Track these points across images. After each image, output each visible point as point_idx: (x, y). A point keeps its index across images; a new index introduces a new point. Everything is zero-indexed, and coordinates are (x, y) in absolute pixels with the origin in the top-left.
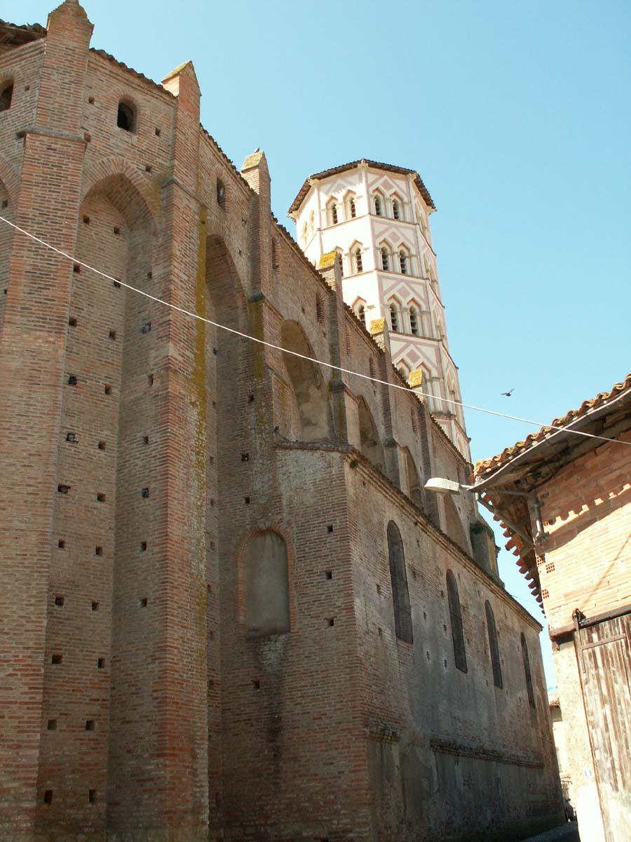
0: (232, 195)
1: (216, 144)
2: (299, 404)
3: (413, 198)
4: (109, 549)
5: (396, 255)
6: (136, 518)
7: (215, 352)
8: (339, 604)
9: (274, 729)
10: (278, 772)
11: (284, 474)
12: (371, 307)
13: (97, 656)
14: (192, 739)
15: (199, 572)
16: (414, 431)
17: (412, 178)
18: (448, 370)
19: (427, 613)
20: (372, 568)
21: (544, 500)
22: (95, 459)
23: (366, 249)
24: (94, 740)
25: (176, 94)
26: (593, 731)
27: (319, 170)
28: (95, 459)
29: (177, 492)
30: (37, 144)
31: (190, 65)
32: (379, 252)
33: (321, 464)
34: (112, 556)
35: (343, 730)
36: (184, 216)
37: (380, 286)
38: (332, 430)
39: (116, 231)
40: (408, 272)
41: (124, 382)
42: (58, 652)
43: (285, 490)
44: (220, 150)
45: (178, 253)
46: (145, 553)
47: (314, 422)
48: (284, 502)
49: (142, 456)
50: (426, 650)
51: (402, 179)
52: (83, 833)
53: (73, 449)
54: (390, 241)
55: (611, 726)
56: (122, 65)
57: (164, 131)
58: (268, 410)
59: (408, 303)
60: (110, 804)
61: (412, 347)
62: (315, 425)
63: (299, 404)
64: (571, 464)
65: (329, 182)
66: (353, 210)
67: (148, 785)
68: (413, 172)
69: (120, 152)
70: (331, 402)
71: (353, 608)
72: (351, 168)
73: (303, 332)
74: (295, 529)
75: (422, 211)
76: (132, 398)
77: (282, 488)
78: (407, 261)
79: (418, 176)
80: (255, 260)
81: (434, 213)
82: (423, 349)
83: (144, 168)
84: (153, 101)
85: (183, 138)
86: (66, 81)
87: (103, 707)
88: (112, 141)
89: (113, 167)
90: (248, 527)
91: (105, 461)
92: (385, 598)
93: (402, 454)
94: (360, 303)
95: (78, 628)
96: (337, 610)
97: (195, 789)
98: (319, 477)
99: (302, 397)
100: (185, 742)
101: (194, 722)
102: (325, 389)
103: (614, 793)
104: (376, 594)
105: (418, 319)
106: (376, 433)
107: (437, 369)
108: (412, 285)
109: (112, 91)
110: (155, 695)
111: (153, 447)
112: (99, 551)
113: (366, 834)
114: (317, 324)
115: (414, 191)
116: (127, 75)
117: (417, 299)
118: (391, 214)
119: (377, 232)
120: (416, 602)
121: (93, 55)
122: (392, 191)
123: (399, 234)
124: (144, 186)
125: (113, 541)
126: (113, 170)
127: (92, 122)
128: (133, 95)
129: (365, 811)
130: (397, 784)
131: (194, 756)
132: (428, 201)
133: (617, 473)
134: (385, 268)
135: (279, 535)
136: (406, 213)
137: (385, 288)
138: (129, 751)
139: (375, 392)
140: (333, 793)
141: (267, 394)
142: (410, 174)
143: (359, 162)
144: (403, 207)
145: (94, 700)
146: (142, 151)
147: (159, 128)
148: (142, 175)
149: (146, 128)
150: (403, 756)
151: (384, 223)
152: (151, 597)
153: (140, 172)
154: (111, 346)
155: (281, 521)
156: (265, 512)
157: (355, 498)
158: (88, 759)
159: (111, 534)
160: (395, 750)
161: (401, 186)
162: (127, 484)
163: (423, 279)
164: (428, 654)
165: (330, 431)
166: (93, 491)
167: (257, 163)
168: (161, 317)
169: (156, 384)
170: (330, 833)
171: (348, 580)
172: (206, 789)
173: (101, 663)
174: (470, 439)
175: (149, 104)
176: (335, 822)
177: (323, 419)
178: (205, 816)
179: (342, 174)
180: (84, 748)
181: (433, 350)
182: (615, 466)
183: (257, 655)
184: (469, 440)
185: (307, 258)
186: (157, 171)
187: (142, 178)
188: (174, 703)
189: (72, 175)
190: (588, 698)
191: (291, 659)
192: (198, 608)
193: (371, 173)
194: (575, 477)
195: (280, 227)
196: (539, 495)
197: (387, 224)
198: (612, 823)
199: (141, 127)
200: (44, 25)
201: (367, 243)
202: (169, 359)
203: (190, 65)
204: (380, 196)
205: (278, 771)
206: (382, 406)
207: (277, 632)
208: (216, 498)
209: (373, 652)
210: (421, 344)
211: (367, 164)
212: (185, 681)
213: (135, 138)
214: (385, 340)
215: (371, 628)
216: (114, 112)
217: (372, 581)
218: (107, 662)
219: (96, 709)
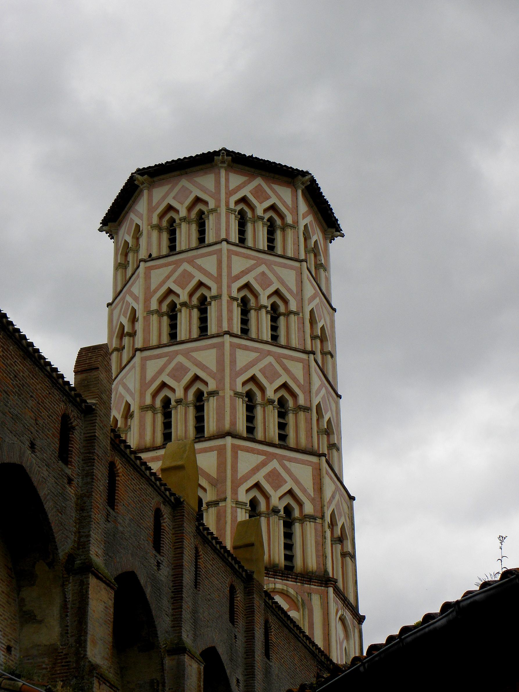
5: (263, 311)
16: (232, 620)
18: (334, 502)
32: (235, 304)
38: (64, 633)
40: (282, 340)
47: (39, 618)
54: (256, 286)
59: (276, 391)
61: (274, 464)
75: (317, 236)
81: (338, 240)
82: (293, 467)
93: (195, 666)
107: (312, 501)
108: (285, 361)
117: (292, 384)
122: (267, 204)
139: (159, 564)
151: (248, 257)
163: (305, 352)
165: (62, 635)
181: (310, 469)
197: (253, 258)
204: (246, 209)
210: (290, 460)
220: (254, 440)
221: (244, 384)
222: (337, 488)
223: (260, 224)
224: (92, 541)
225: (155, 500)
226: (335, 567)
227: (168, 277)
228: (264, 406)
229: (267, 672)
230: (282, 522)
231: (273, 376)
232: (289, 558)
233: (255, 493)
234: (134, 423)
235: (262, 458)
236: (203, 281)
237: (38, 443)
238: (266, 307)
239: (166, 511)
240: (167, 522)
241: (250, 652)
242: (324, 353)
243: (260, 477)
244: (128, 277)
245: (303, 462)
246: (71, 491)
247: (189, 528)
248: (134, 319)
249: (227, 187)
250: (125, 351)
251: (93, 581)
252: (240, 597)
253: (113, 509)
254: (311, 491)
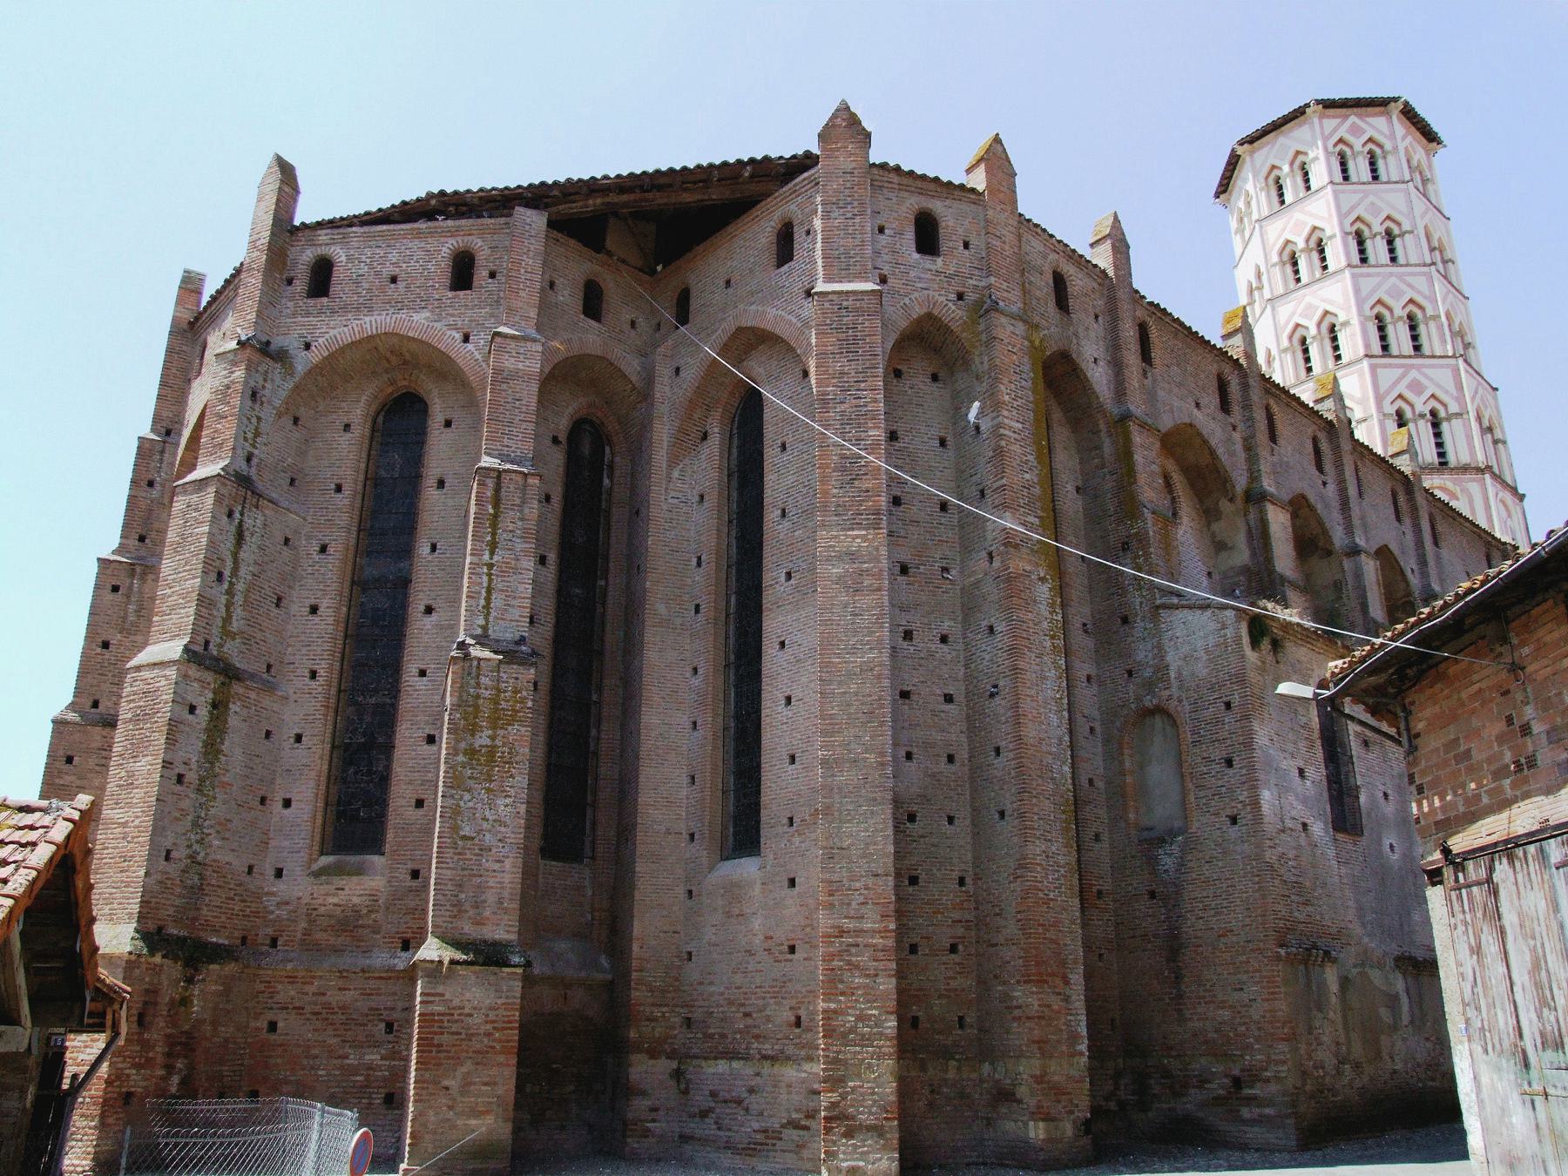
0: (1076, 288)
1: (1044, 230)
2: (1209, 524)
3: (1399, 140)
4: (963, 754)
5: (1378, 237)
6: (988, 719)
7: (1078, 489)
8: (1241, 798)
9: (1174, 946)
10: (1181, 998)
11: (1171, 640)
12: (1346, 324)
13: (956, 875)
14: (1063, 963)
15: (1063, 775)
16: (1398, 519)
17: (1395, 109)
19: (1389, 792)
20: (1290, 747)
21: (1413, 708)
22: (937, 655)
23: (1331, 238)
24: (958, 964)
25: (981, 187)
26: (1463, 984)
27: (1249, 129)
28: (937, 655)
29: (1029, 688)
30: (827, 305)
31: (997, 140)
32: (1350, 237)
33: (1213, 626)
34: (966, 762)
35: (1252, 950)
36: (1010, 348)
37: (1357, 291)
38: (1253, 555)
39: (935, 378)
41: (962, 561)
42: (914, 873)
43: (1173, 659)
44: (1052, 236)
45: (1007, 398)
46: (1000, 759)
48: (1173, 675)
49: (988, 648)
50: (1386, 842)
51: (1381, 114)
52: (954, 1059)
53: (912, 648)
55: (1479, 980)
56: (911, 173)
57: (973, 241)
58: (1146, 560)
60: (980, 1030)
62: (1231, 548)
63: (1209, 524)
64: (1433, 671)
65: (1268, 143)
66: (1307, 181)
67: (1016, 1013)
68: (1395, 100)
69: (924, 286)
70: (1252, 516)
71: (1259, 803)
72: (1297, 117)
73: (1200, 434)
74: (1188, 707)
75: (1419, 154)
76: (972, 579)
77: (1169, 658)
78: (1398, 242)
79: (1406, 104)
80: (1117, 365)
81: (1441, 151)
83: (953, 297)
84: (956, 204)
85: (998, 244)
86: (849, 215)
87: (968, 928)
88: (912, 274)
89: (917, 309)
90: (1133, 706)
91: (949, 657)
92: (1313, 782)
93: (1372, 563)
94: (1329, 319)
95: (933, 845)
96: (1240, 806)
97: (1069, 1017)
98: (1212, 641)
99: (1209, 514)
100: (1055, 967)
101: (1066, 945)
102: (1239, 501)
103: (1484, 1056)
104: (1298, 779)
105: (1422, 329)
106: (1329, 539)
108: (1408, 278)
109: (904, 209)
110: (1019, 916)
111: (999, 638)
112: (951, 759)
113: (1284, 1075)
114: (1221, 416)
115: (1400, 127)
116: (919, 183)
118: (1366, 175)
119: (1344, 210)
120: (1368, 780)
121: (875, 171)
123: (1379, 203)
124: (957, 321)
125: (966, 746)
126: (918, 311)
127: (886, 258)
128: (930, 206)
129: (1283, 1046)
130: (1335, 1014)
131: (1067, 982)
132: (1429, 136)
133: (1476, 687)
134: (1364, 260)
135: (1169, 715)
136: (1391, 168)
137: (1364, 293)
138: (996, 977)
139: (1324, 484)
140: (1245, 1023)
141: (1142, 539)
142: (1393, 104)
143: (1308, 105)
144: (1385, 158)
145: (957, 921)
146: (950, 277)
147: (967, 239)
148: (953, 308)
149: (951, 244)
150: (1345, 982)
152: (1009, 809)
153: (950, 304)
154: (943, 520)
155: (1170, 697)
156: (1150, 686)
157: (1259, 663)
158: (953, 984)
159: (963, 738)
160: (1331, 976)
161: (1378, 126)
162: (975, 681)
164: (1391, 846)
166: (938, 692)
167: (1107, 232)
168: (995, 482)
169: (997, 563)
170: (1242, 1071)
171: (1251, 768)
172: (1084, 1018)
173: (962, 882)
174: (1524, 495)
175: (950, 210)
176: (1248, 1057)
177: (1241, 539)
178: (1083, 1047)
179: (1283, 128)
180: (950, 974)
182: (1475, 677)
183: (1152, 861)
184: (1522, 497)
185: (1196, 333)
186: (971, 297)
187: (953, 312)
188: (1039, 925)
189: (869, 335)
190: (1456, 946)
191: (1190, 865)
192: (1064, 816)
193: (1329, 117)
194: (1439, 686)
195: (1151, 304)
196: (1407, 701)
197: (1359, 191)
198: (1484, 1089)
199: (944, 246)
200: (816, 150)
201: (1332, 228)
202: (1008, 533)
203: (997, 140)
204: (1347, 150)
205: (1180, 996)
206: (1338, 498)
207: (1173, 833)
208: (1093, 672)
209: (1291, 854)
211: (1321, 106)
212: (1052, 900)
213: (939, 260)
214: (1335, 405)
215: (1289, 824)
216: (910, 235)
217: (1290, 765)
218: (968, 880)
219: (960, 931)
220: (1391, 356)
221: (1352, 224)
222: (1479, 383)
223: (1400, 324)
224: (1263, 474)
225: (1310, 429)
226: (1457, 294)
227: (1284, 230)
228: (1394, 324)
229: (1438, 558)
230: (1429, 424)
231: (1397, 294)
232: (1441, 455)
233: (1400, 403)
234: (1276, 364)
235: (1401, 371)
236: (1317, 225)
237: (1202, 402)
238: (1381, 233)
239: (1322, 436)
240: (1325, 446)
241: (1419, 544)
242: (1445, 262)
243: (1401, 388)
244: (1247, 238)
245: (1442, 366)
246: (1237, 436)
247: (1346, 446)
248: (1259, 276)
249: (1322, 133)
250: (1257, 304)
251: (1270, 509)
252: (1402, 499)
253: (1276, 444)
254: (1453, 391)
